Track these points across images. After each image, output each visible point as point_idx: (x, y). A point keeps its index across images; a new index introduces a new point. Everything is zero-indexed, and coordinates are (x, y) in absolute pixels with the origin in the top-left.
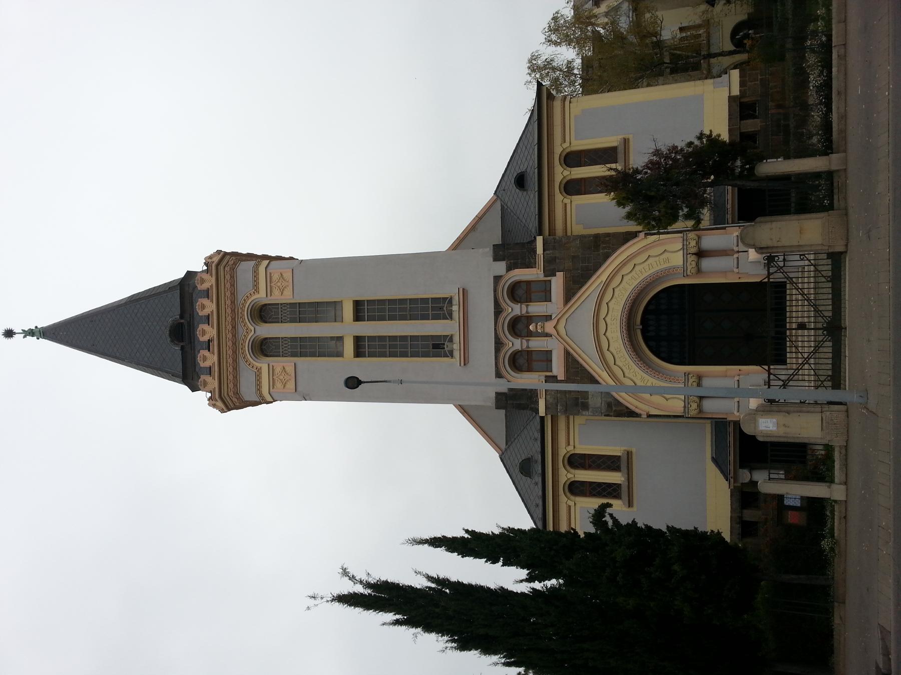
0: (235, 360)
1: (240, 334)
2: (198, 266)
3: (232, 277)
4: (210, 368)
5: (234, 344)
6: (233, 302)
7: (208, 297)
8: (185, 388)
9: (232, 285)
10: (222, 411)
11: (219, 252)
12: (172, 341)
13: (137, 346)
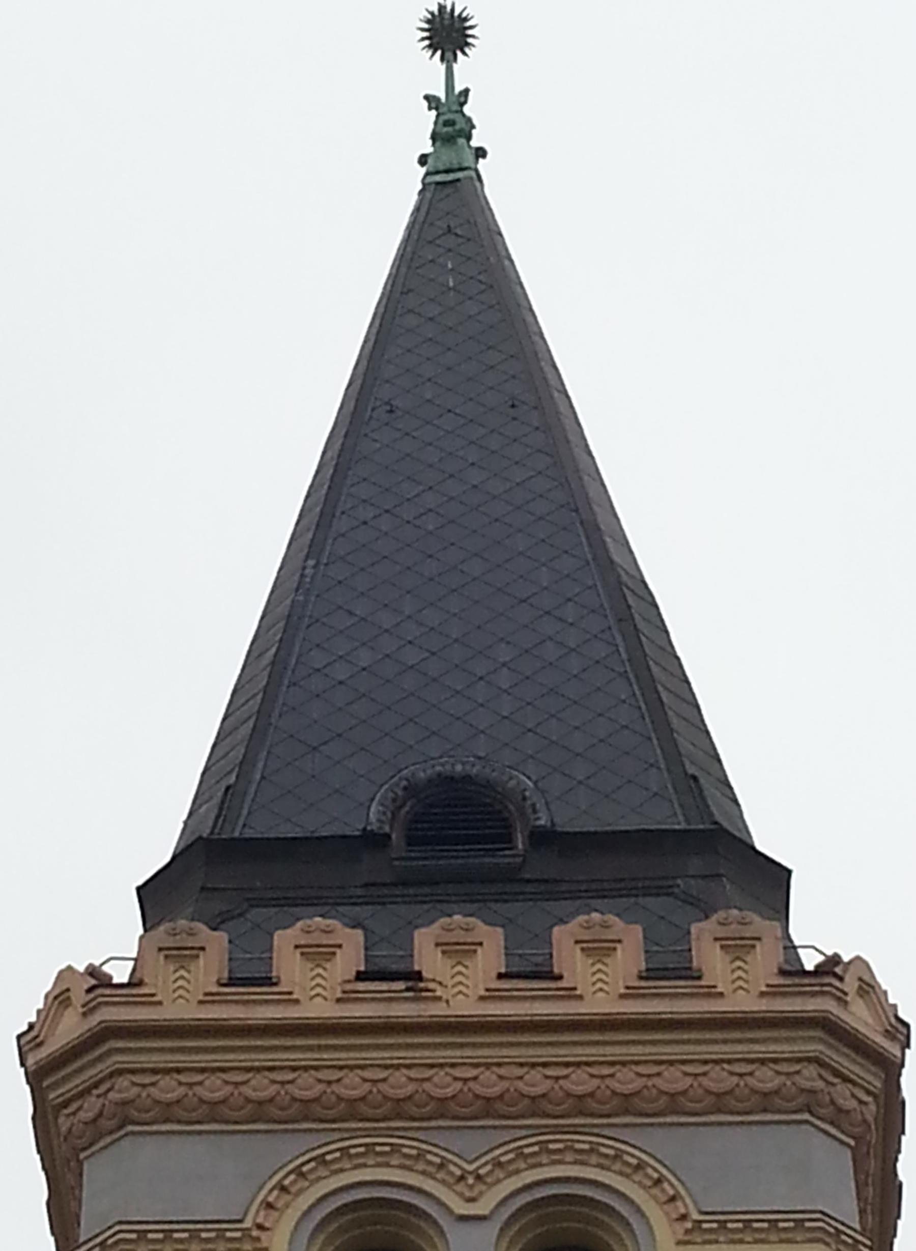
0: (306, 1111)
1: (457, 1141)
2: (816, 927)
3: (766, 1101)
4: (268, 981)
5: (399, 1109)
6: (627, 1103)
7: (649, 974)
8: (156, 846)
9: (720, 1102)
10: (28, 1042)
11: (900, 1032)
12: (411, 789)
13: (386, 619)
